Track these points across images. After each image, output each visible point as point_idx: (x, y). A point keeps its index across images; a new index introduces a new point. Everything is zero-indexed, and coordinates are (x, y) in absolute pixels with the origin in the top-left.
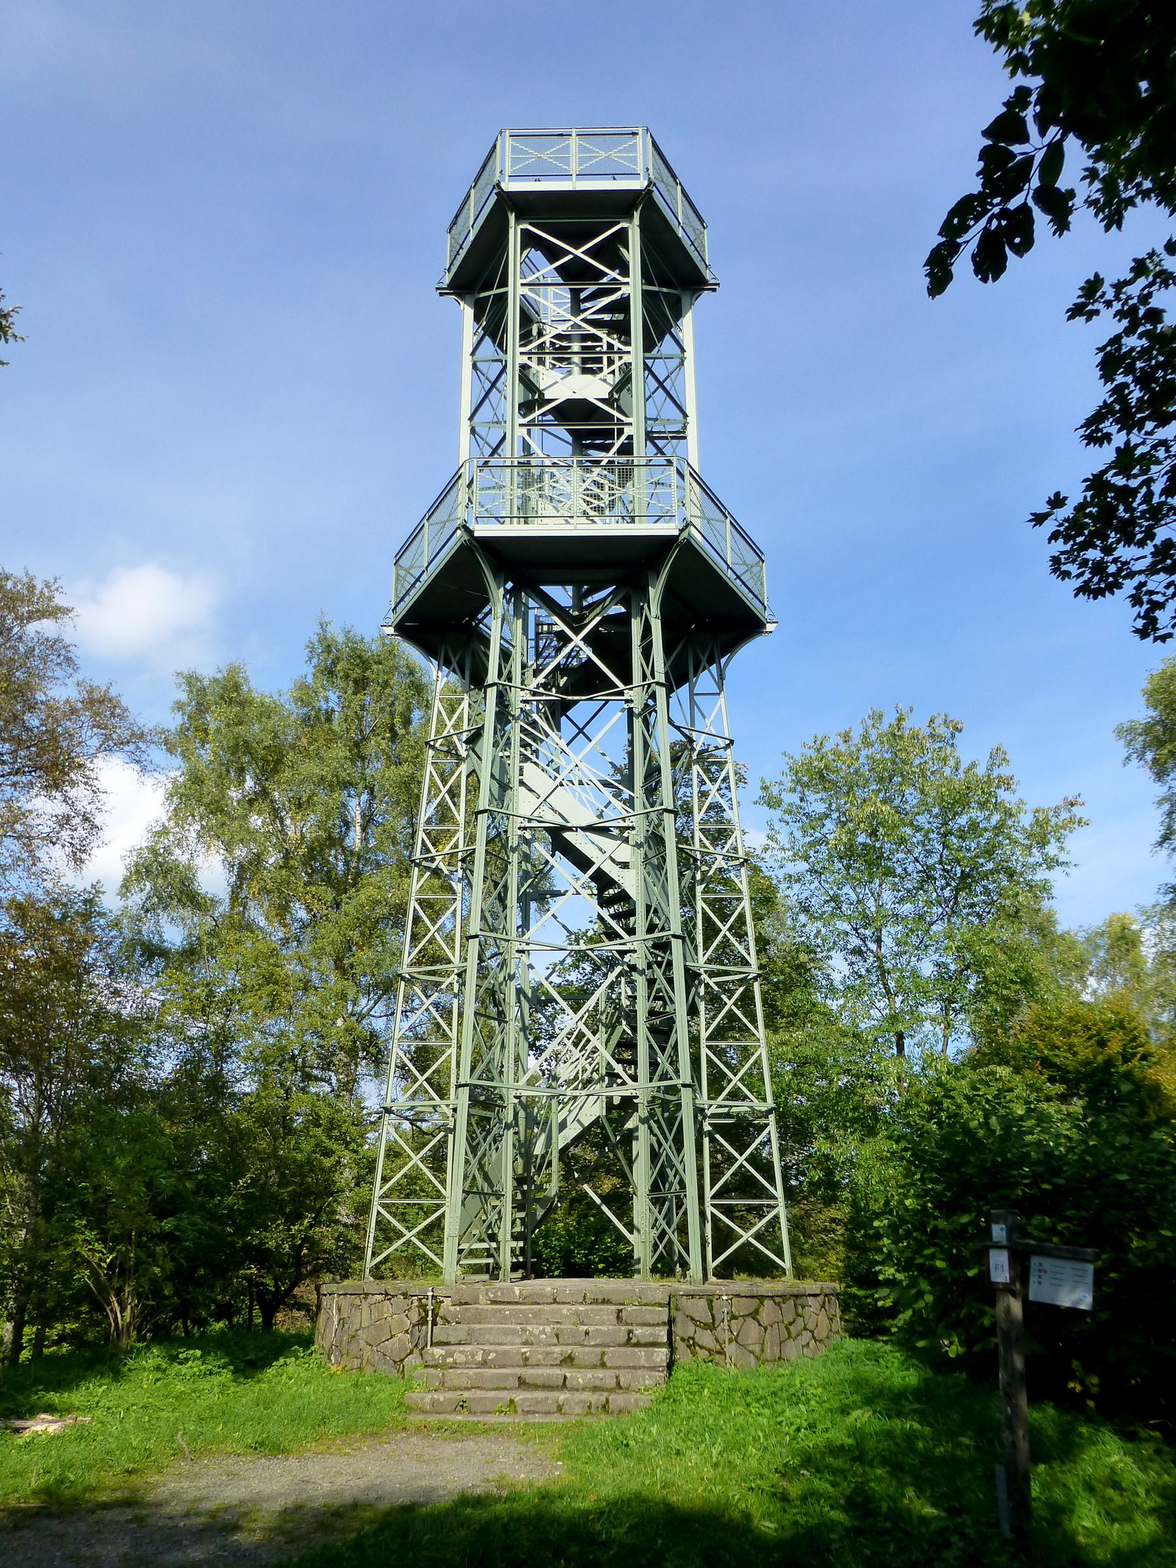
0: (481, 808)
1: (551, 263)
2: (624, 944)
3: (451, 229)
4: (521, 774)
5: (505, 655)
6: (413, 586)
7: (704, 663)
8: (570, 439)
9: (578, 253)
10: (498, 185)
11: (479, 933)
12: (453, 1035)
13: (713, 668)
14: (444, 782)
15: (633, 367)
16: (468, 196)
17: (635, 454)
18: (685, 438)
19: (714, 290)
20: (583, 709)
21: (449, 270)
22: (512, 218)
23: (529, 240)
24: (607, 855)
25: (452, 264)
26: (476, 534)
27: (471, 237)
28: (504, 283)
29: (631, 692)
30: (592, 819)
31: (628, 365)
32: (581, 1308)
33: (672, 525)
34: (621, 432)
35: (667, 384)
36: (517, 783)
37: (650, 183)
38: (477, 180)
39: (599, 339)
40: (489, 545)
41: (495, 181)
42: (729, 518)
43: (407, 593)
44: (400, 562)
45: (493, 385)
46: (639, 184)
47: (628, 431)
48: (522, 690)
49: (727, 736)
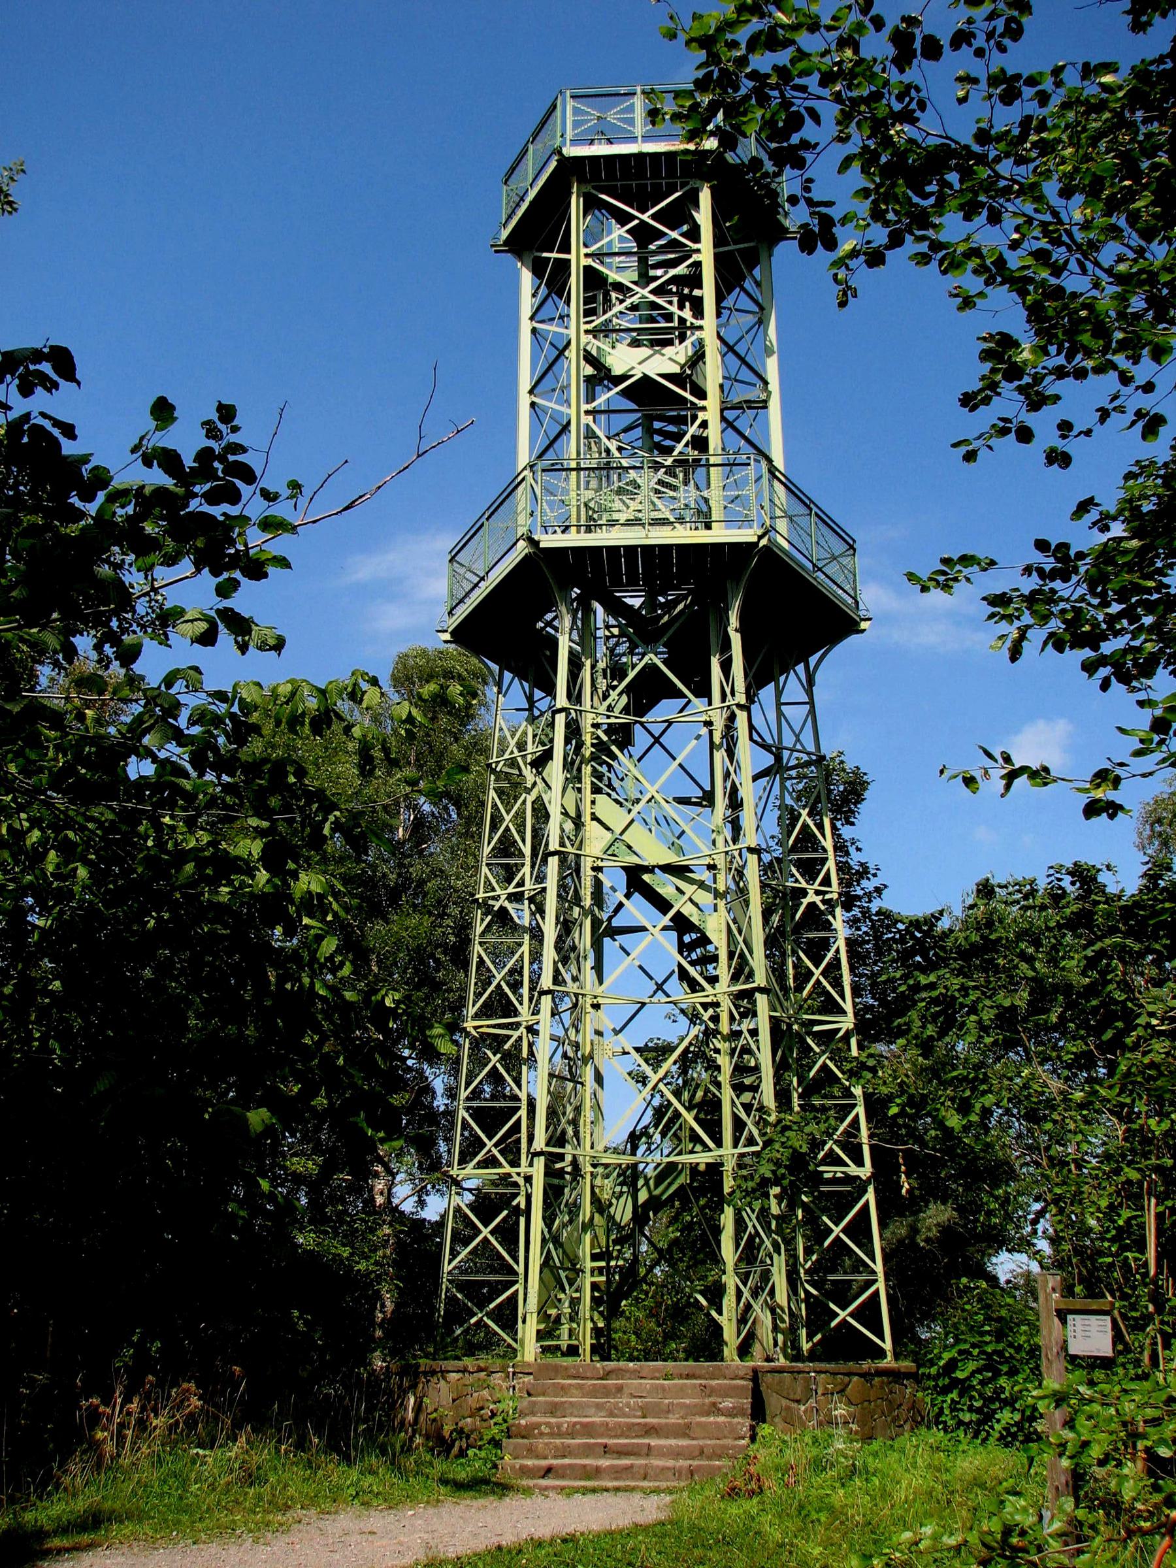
9: (508, 818)
12: (520, 1269)
13: (800, 668)
16: (524, 152)
17: (711, 451)
26: (542, 545)
33: (751, 531)
34: (695, 418)
36: (588, 817)
38: (535, 135)
42: (815, 509)
43: (467, 594)
47: (701, 416)
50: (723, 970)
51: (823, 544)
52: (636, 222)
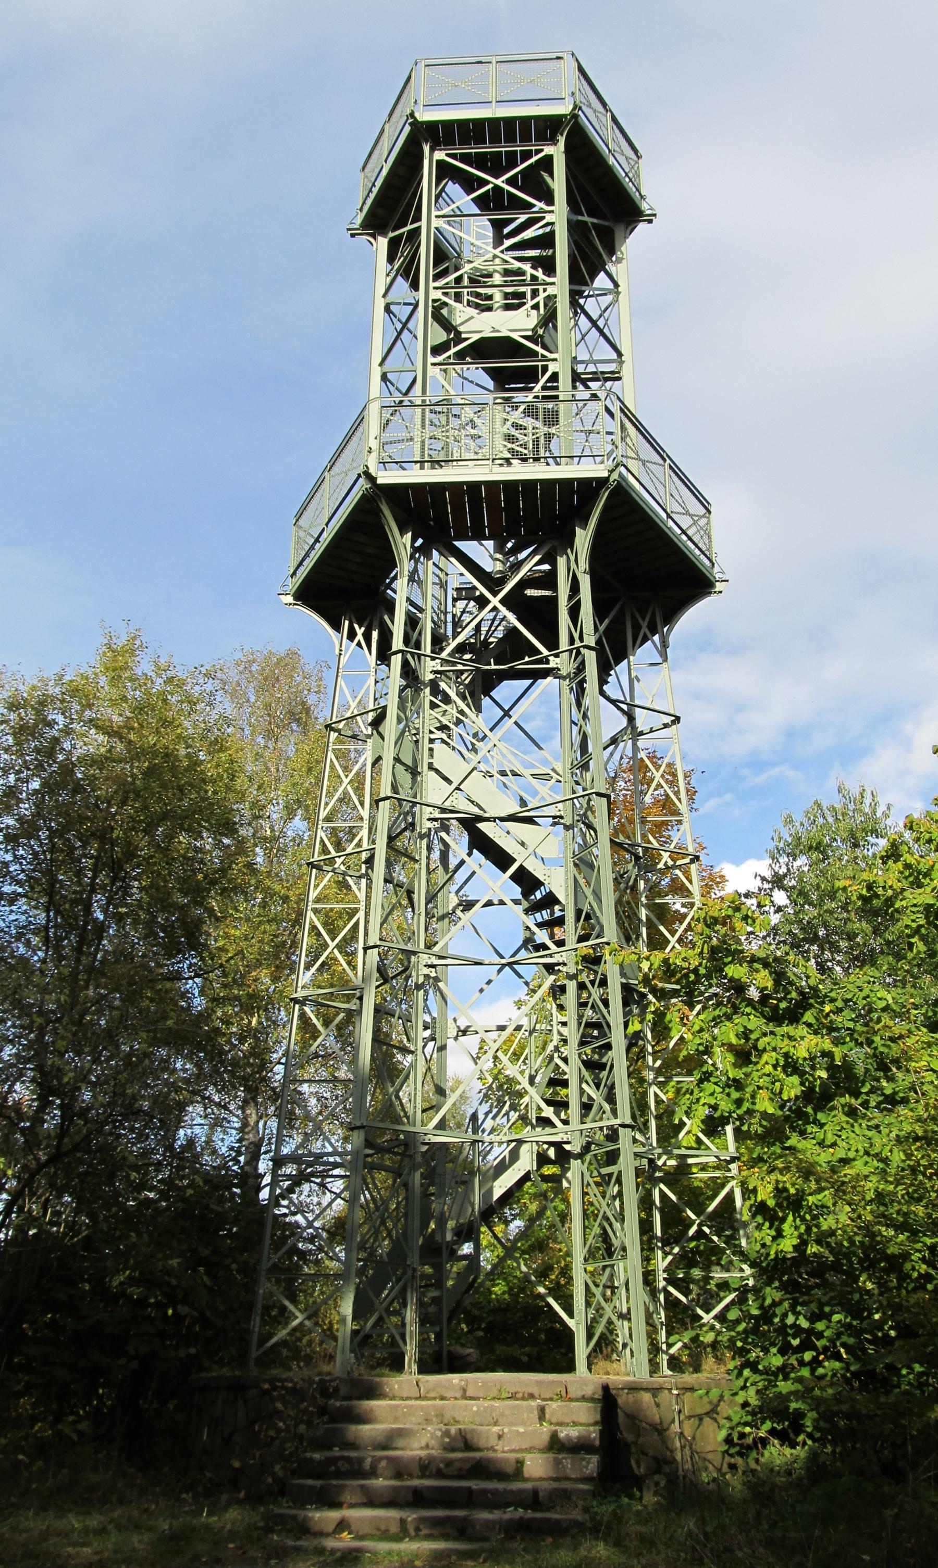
0: (382, 795)
1: (468, 194)
2: (551, 956)
3: (364, 168)
4: (432, 756)
5: (412, 622)
6: (312, 547)
7: (645, 630)
8: (490, 384)
10: (412, 115)
11: (378, 943)
13: (656, 638)
14: (346, 769)
15: (558, 299)
16: (382, 131)
18: (619, 379)
19: (650, 221)
20: (507, 690)
21: (361, 210)
22: (426, 149)
23: (444, 171)
24: (530, 850)
25: (364, 203)
26: (379, 481)
27: (385, 172)
28: (418, 218)
29: (557, 660)
30: (515, 808)
31: (550, 299)
32: (497, 1404)
34: (545, 369)
35: (601, 323)
36: (426, 767)
37: (575, 107)
38: (390, 115)
39: (523, 273)
40: (395, 493)
41: (409, 112)
42: (668, 461)
44: (301, 522)
45: (405, 325)
46: (563, 109)
47: (552, 367)
48: (433, 659)
49: (672, 712)
50: (570, 932)
51: (677, 497)
52: (490, 186)
